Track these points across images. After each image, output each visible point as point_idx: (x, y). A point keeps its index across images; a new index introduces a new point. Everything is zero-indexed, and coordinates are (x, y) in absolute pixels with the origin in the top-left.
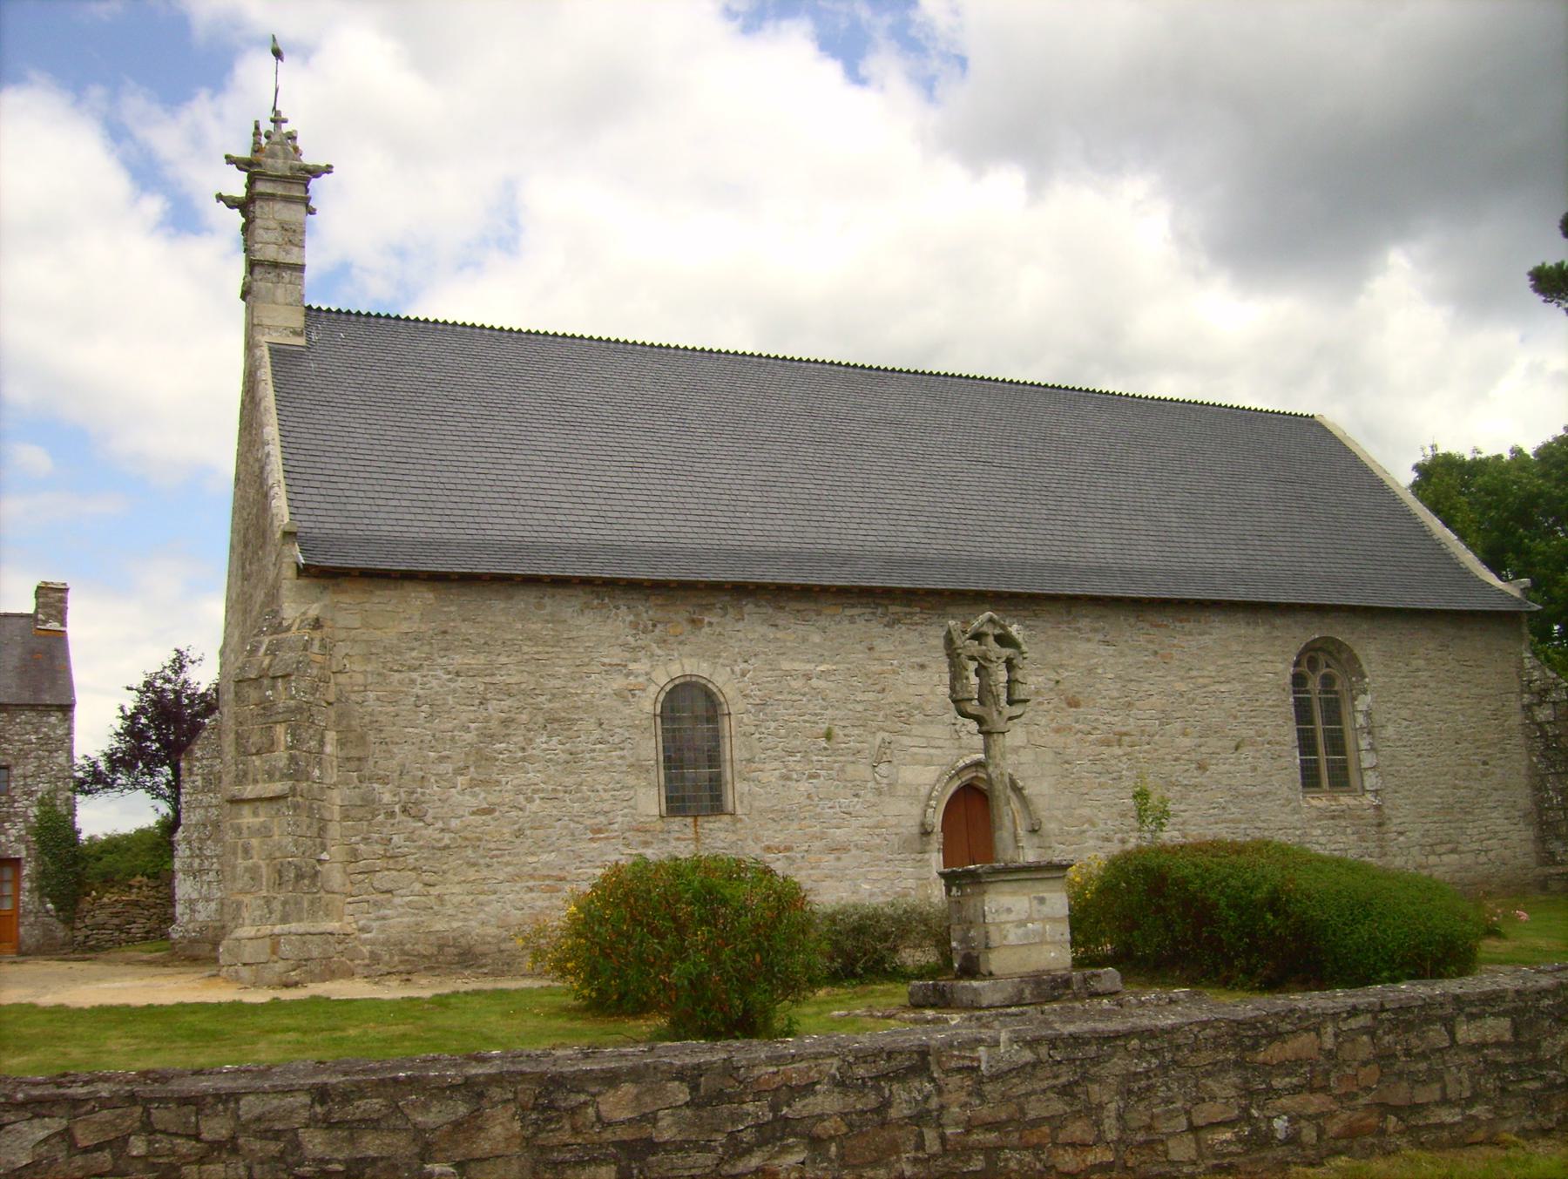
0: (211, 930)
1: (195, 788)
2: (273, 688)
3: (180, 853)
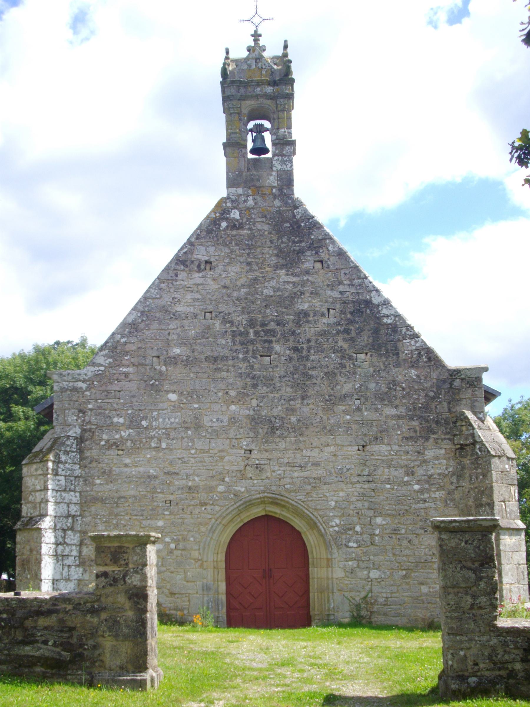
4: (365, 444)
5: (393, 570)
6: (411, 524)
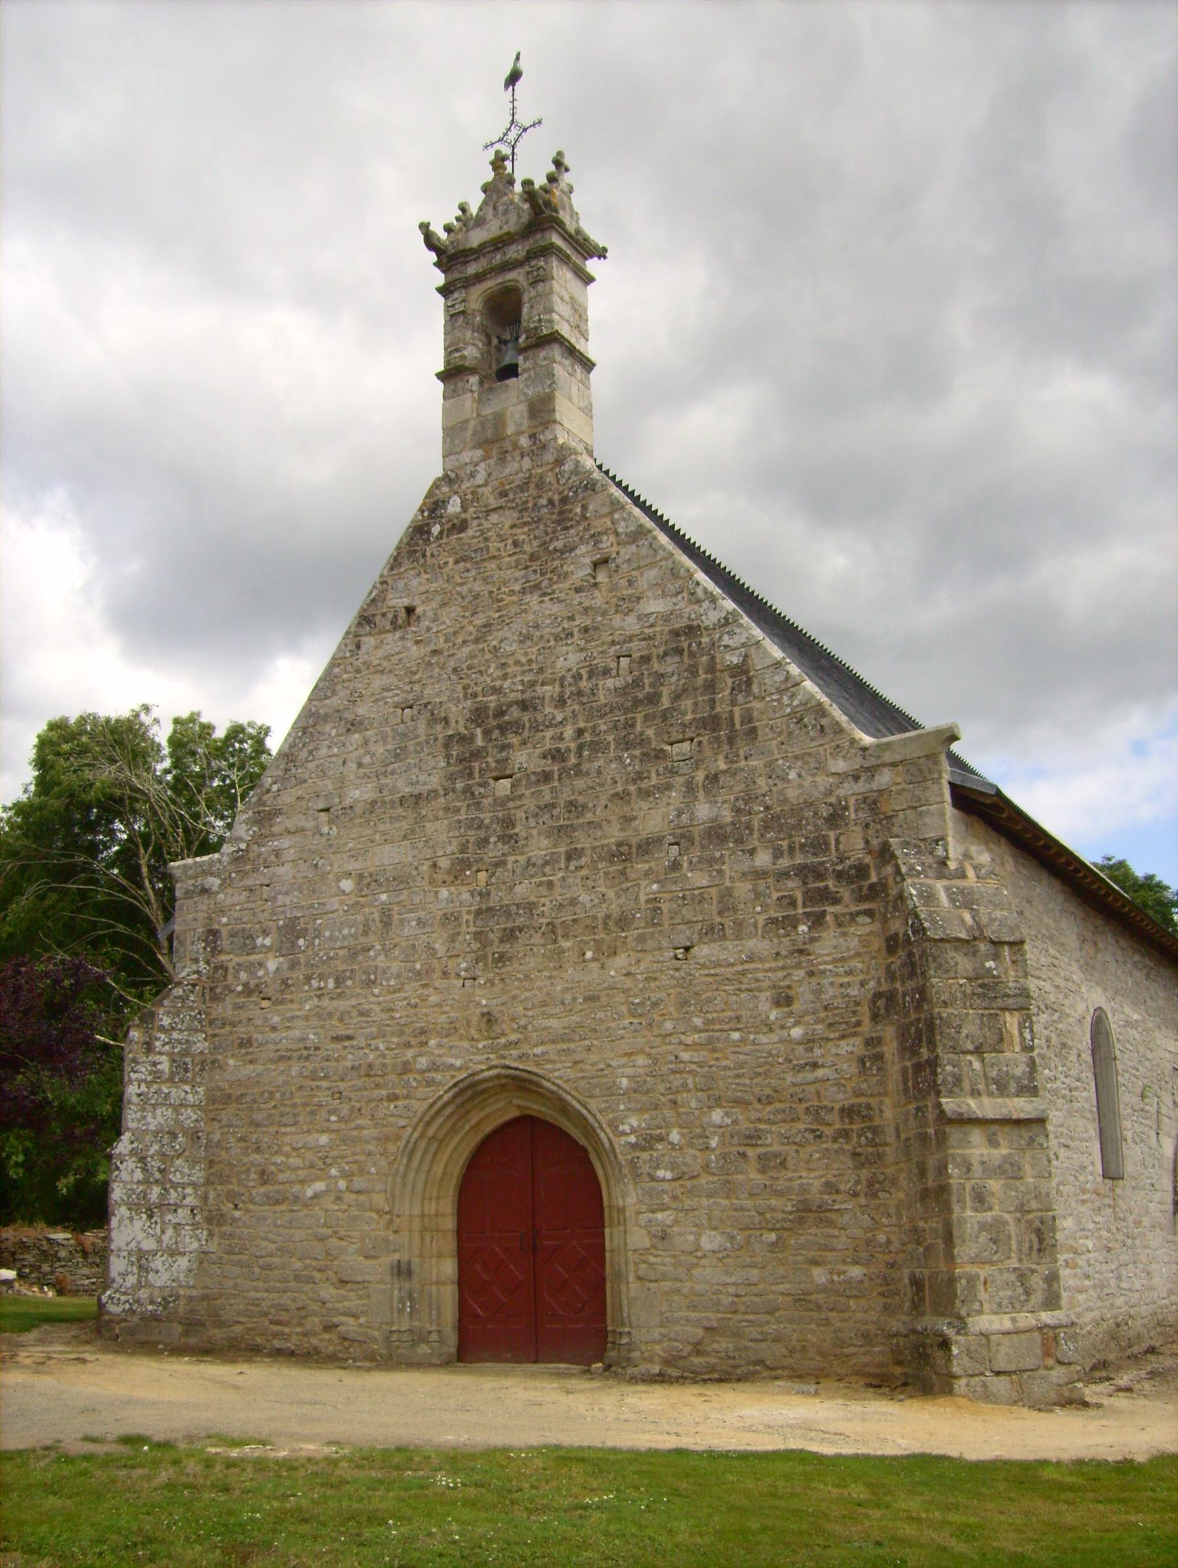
0: (182, 1302)
1: (157, 1076)
2: (996, 957)
3: (125, 1175)
4: (688, 944)
5: (749, 1232)
6: (784, 1121)
